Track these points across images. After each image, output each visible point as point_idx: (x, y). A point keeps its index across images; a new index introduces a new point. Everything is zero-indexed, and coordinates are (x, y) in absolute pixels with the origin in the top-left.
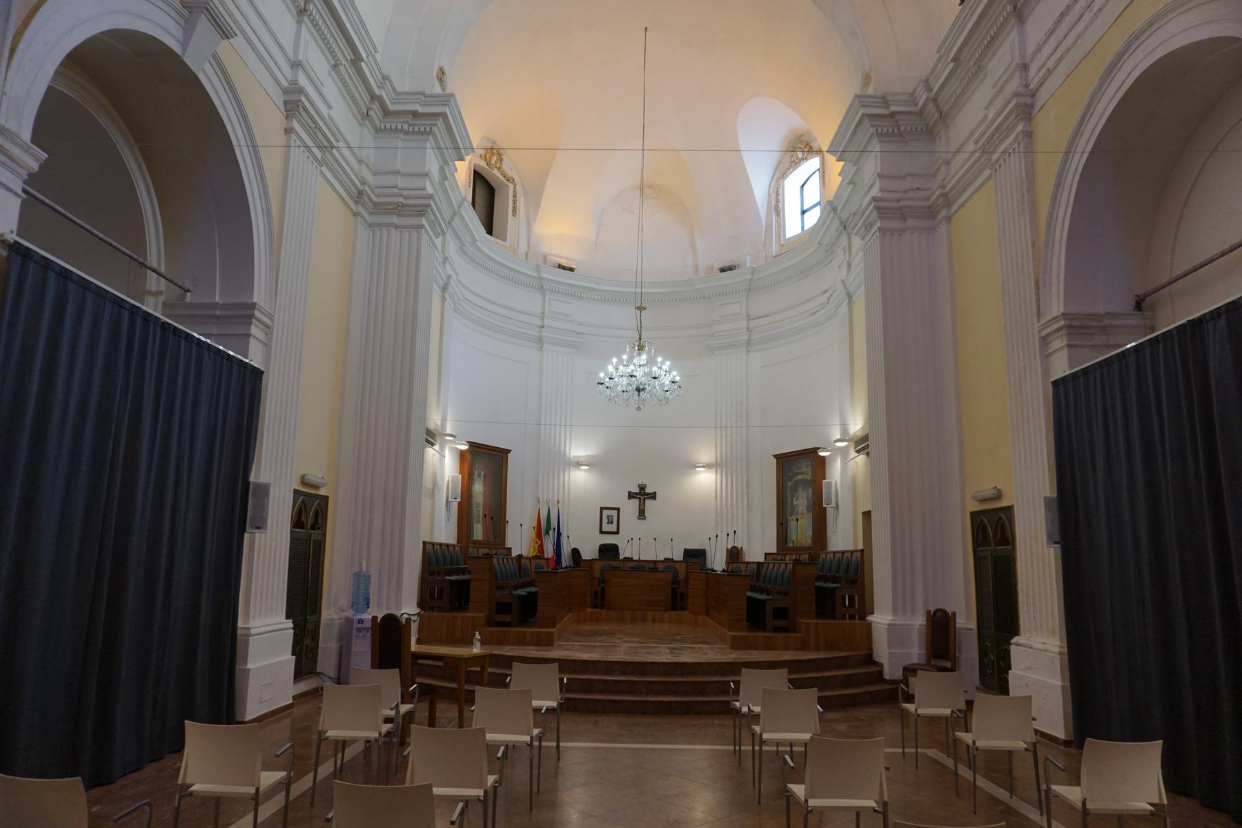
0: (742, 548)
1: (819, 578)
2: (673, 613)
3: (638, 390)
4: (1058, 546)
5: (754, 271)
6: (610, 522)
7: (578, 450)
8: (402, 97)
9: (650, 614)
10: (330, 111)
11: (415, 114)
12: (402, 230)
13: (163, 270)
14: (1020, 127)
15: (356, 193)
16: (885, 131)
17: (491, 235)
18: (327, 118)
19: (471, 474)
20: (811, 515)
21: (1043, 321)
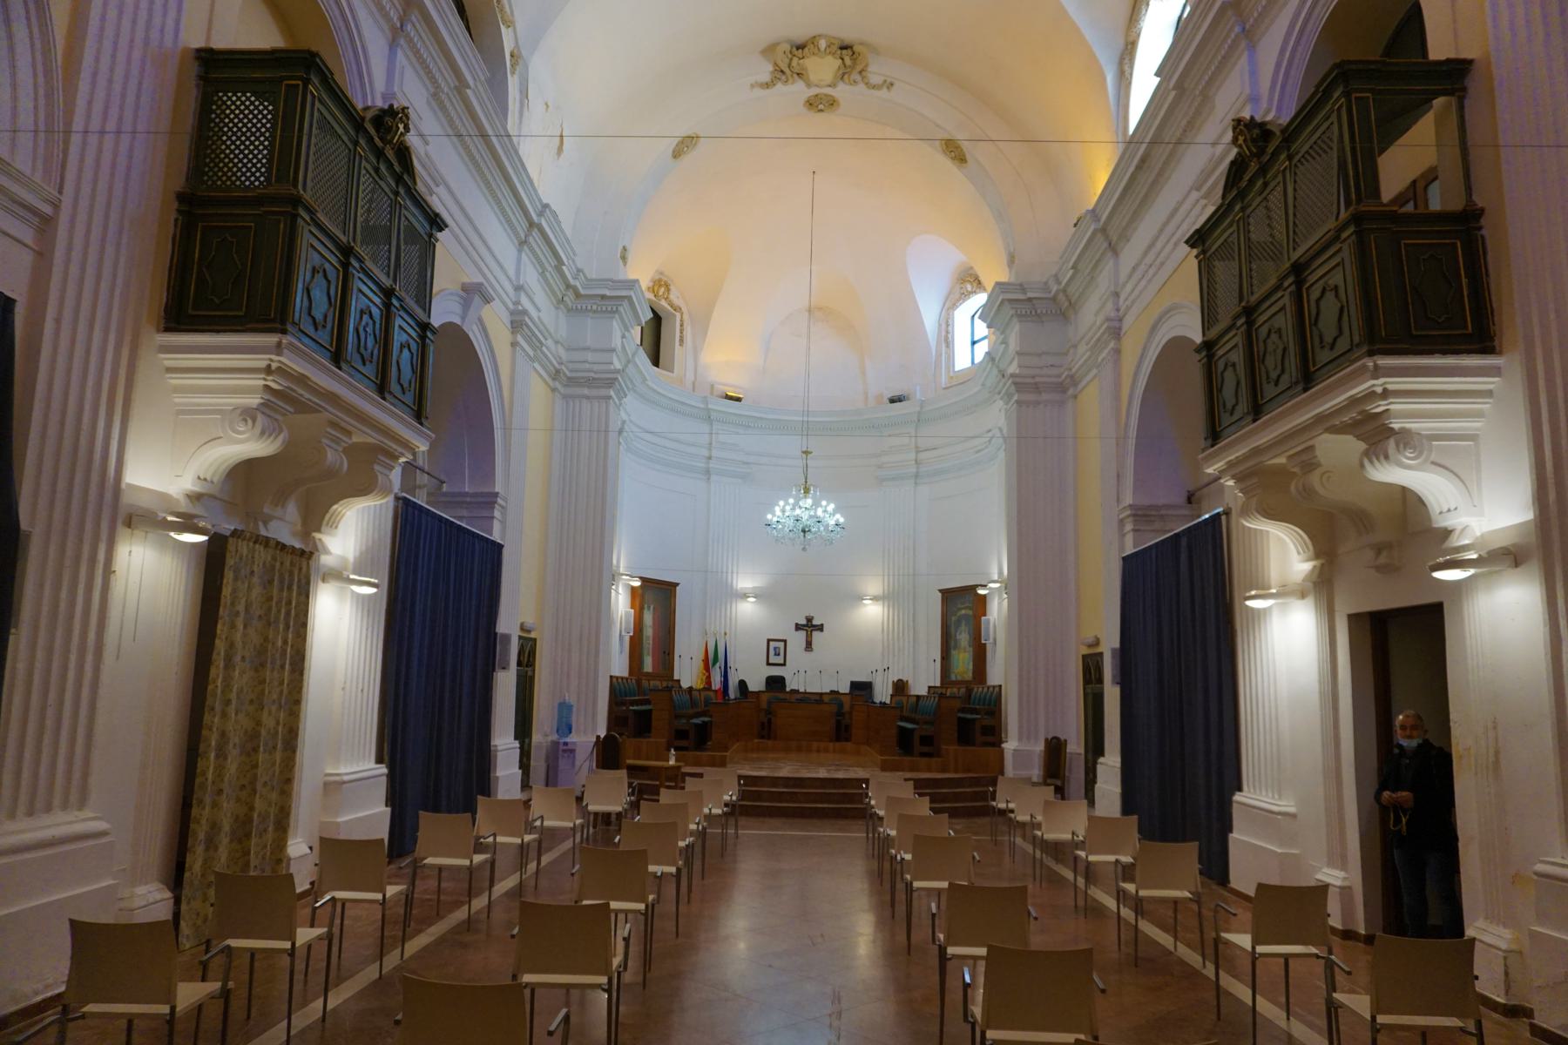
2: (838, 744)
3: (804, 531)
5: (922, 403)
7: (745, 582)
9: (815, 745)
11: (603, 297)
13: (426, 468)
18: (423, 156)
19: (642, 609)
21: (1121, 507)
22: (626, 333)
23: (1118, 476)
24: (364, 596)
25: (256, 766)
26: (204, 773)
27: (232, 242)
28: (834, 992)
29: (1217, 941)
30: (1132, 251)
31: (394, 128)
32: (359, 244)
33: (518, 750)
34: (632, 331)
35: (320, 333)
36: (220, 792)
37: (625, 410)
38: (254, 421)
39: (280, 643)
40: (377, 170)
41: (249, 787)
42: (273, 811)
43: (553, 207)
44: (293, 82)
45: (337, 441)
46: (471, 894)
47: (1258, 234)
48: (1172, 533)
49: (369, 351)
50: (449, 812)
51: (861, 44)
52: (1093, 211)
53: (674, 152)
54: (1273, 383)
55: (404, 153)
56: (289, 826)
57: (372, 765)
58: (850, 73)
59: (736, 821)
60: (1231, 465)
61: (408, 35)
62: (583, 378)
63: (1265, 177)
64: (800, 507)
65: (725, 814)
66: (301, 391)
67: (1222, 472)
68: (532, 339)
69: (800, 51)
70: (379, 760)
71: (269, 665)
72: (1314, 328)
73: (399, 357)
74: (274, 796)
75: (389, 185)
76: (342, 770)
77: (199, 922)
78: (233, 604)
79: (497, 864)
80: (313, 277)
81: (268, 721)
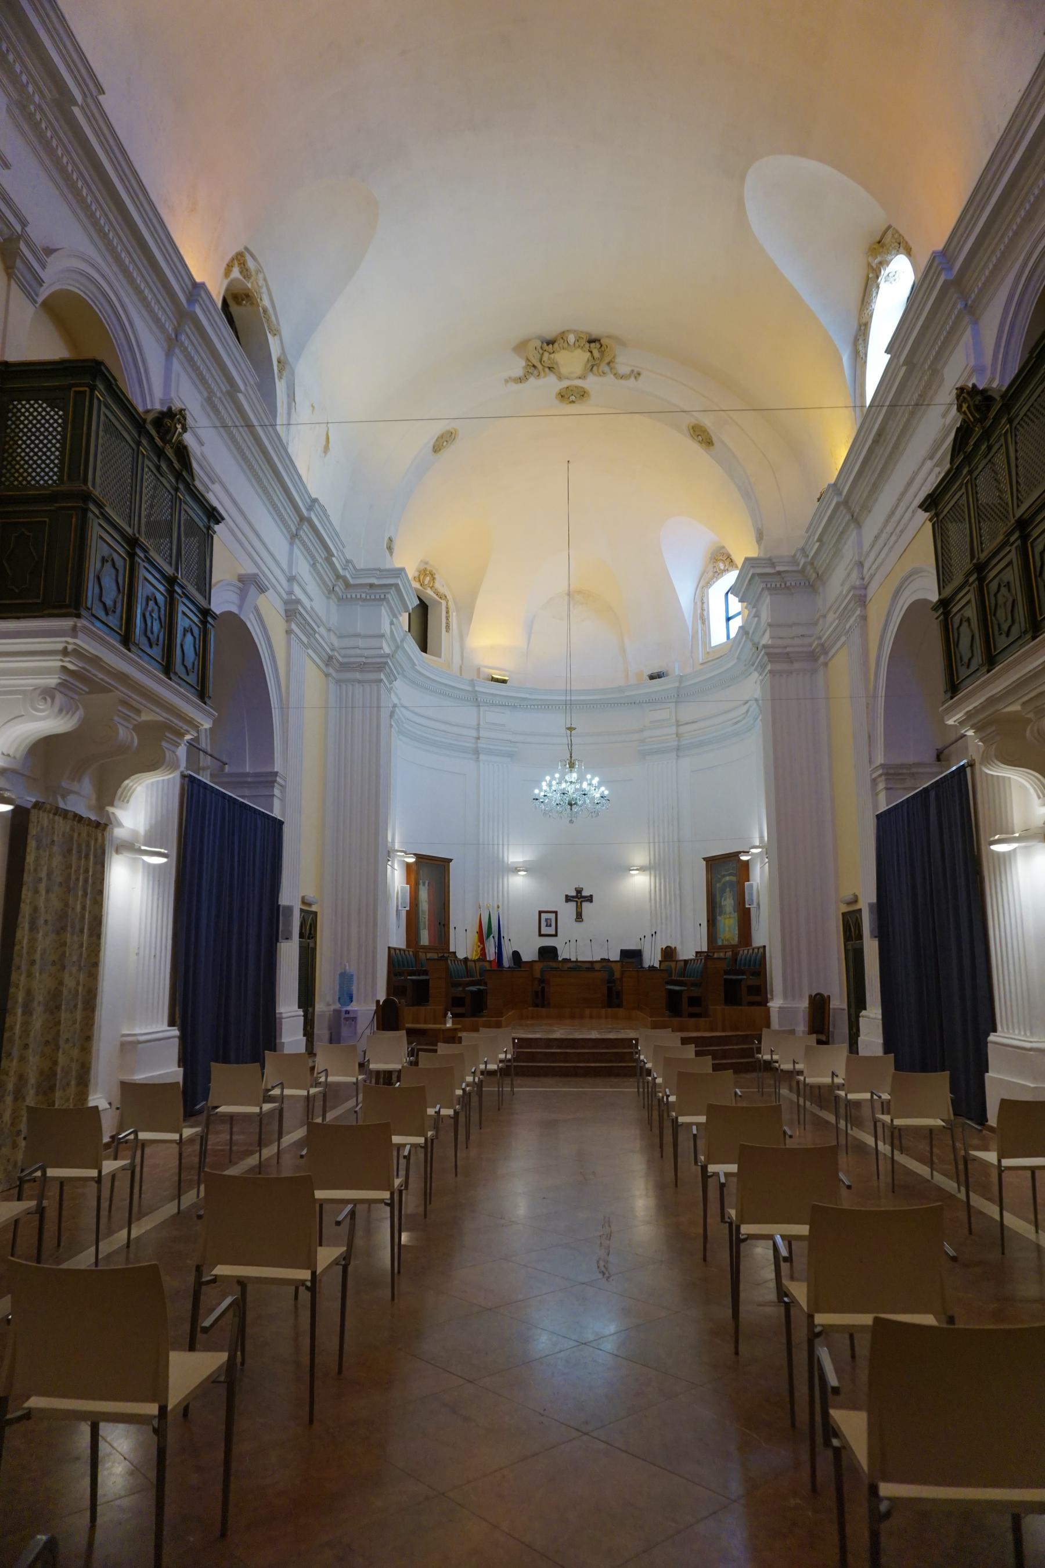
0: (675, 948)
1: (726, 973)
2: (609, 1010)
3: (570, 804)
4: (877, 939)
5: (681, 679)
6: (549, 925)
7: (515, 857)
8: (361, 573)
9: (587, 1011)
10: (202, 447)
11: (371, 586)
12: (364, 684)
13: (209, 750)
14: (858, 612)
15: (327, 657)
16: (773, 585)
17: (426, 652)
18: (201, 457)
19: (417, 884)
20: (736, 914)
21: (873, 766)
22: (394, 620)
23: (869, 737)
24: (155, 867)
25: (59, 1023)
26: (12, 1028)
27: (29, 536)
28: (605, 1217)
29: (966, 1160)
30: (873, 523)
31: (173, 429)
32: (143, 535)
33: (302, 1018)
34: (401, 618)
35: (111, 618)
36: (26, 1046)
37: (396, 694)
38: (53, 698)
39: (78, 908)
40: (158, 468)
41: (52, 1043)
42: (74, 1066)
43: (322, 501)
44: (81, 389)
45: (126, 718)
46: (261, 1144)
47: (987, 496)
48: (921, 788)
49: (156, 635)
50: (237, 1063)
51: (609, 337)
52: (835, 484)
53: (434, 447)
54: (1004, 635)
55: (183, 452)
56: (89, 1081)
57: (165, 1027)
58: (598, 366)
59: (512, 1081)
60: (969, 715)
61: (182, 344)
62: (354, 663)
63: (989, 441)
64: (566, 782)
65: (500, 1070)
66: (94, 672)
67: (962, 723)
68: (306, 628)
69: (551, 346)
70: (172, 1023)
71: (69, 928)
72: (1039, 579)
73: (183, 641)
74: (75, 1052)
75: (169, 482)
76: (137, 1031)
77: (10, 1168)
78: (35, 870)
79: (286, 1114)
80: (103, 566)
81: (69, 982)
